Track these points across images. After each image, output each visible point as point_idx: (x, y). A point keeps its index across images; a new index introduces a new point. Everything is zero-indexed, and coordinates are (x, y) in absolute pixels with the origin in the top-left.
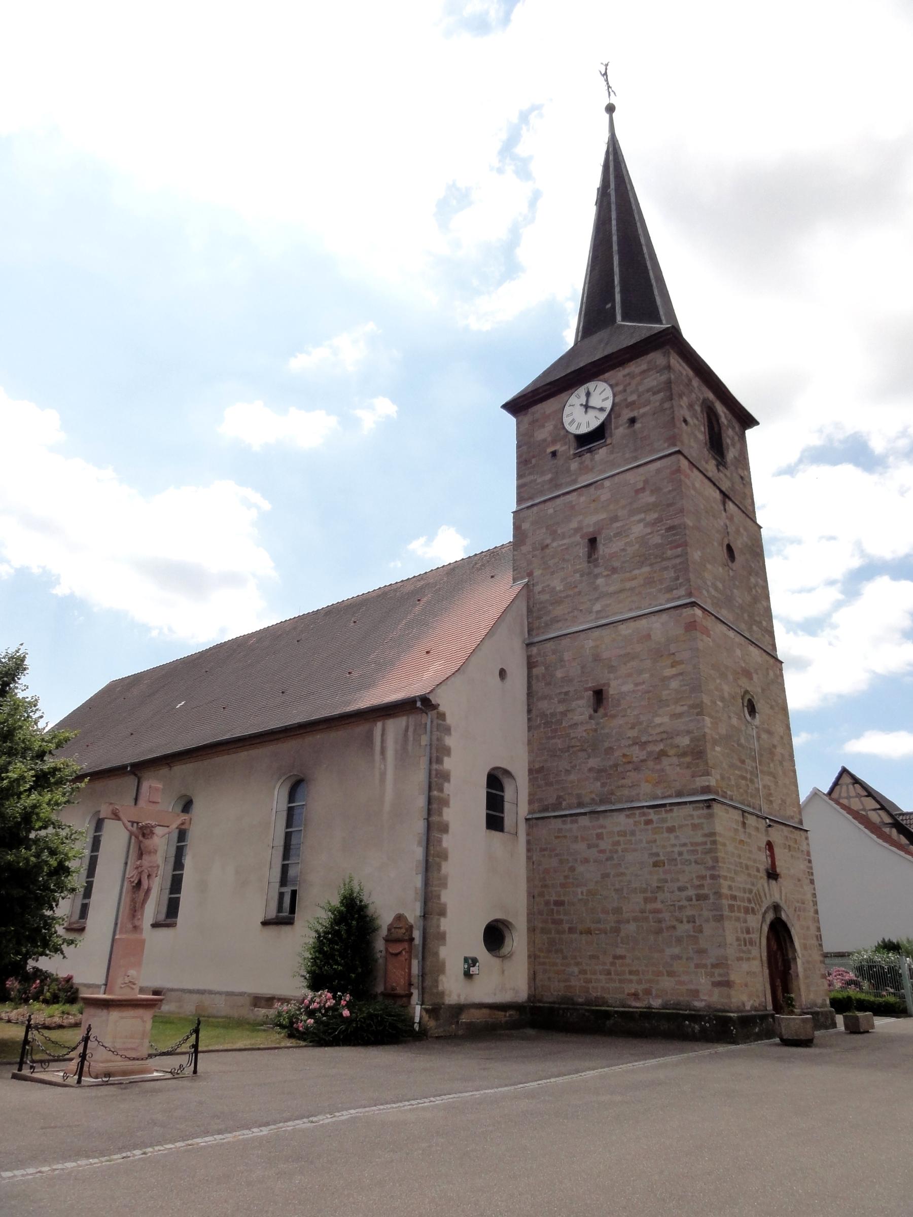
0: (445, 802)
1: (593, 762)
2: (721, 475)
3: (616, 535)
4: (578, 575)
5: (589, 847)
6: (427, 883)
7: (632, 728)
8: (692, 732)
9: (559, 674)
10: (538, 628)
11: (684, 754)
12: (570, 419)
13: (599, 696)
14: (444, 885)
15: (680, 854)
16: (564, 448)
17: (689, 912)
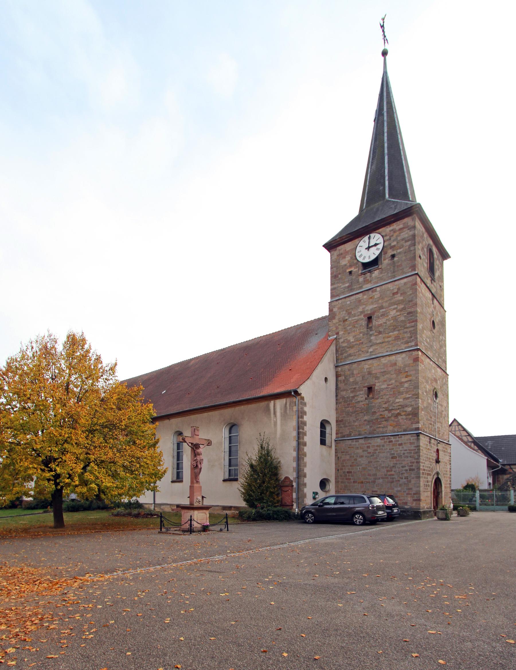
0: (305, 434)
1: (366, 418)
2: (432, 285)
3: (382, 316)
4: (361, 335)
5: (363, 451)
6: (298, 465)
7: (385, 403)
8: (413, 406)
9: (351, 380)
10: (342, 359)
11: (409, 415)
12: (360, 254)
13: (370, 389)
14: (305, 466)
15: (404, 454)
16: (356, 270)
17: (406, 475)
